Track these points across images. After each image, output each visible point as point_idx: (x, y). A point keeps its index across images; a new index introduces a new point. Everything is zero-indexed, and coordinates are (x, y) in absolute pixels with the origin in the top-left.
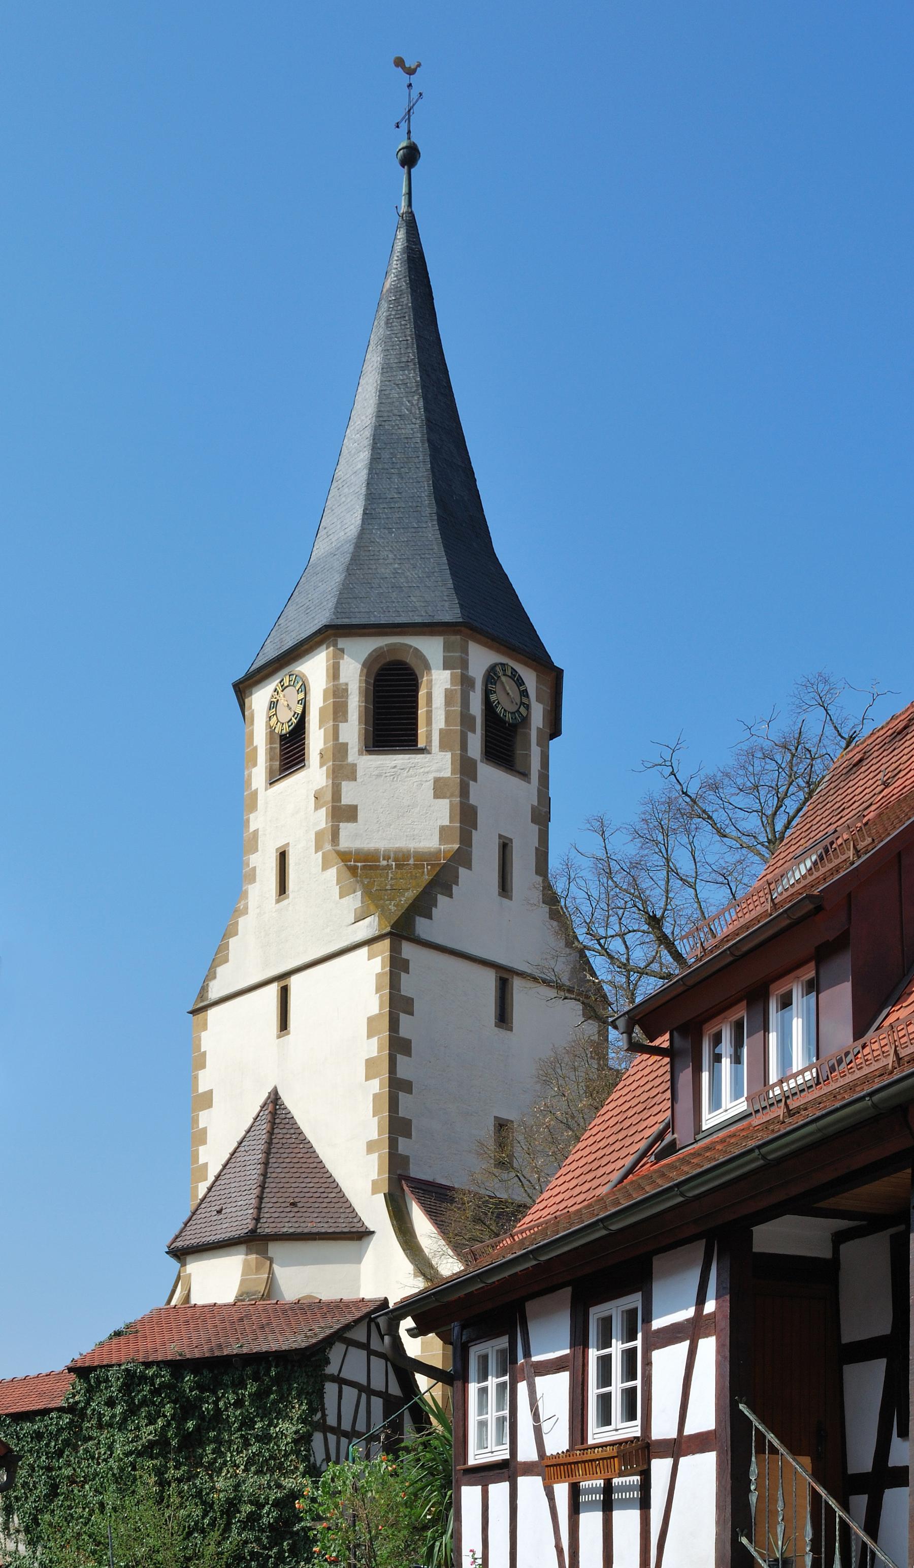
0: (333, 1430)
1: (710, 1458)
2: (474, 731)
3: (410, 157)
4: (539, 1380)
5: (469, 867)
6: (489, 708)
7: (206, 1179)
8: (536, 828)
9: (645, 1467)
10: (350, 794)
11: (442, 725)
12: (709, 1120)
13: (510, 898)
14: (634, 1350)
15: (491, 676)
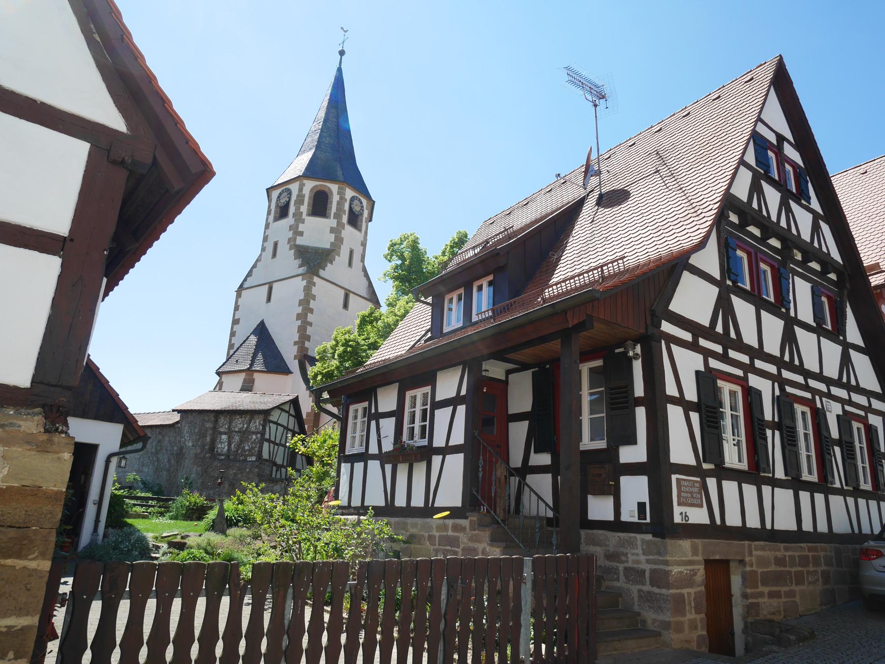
0: (273, 442)
1: (461, 456)
3: (342, 53)
6: (351, 209)
7: (233, 349)
8: (362, 248)
10: (301, 228)
15: (353, 199)
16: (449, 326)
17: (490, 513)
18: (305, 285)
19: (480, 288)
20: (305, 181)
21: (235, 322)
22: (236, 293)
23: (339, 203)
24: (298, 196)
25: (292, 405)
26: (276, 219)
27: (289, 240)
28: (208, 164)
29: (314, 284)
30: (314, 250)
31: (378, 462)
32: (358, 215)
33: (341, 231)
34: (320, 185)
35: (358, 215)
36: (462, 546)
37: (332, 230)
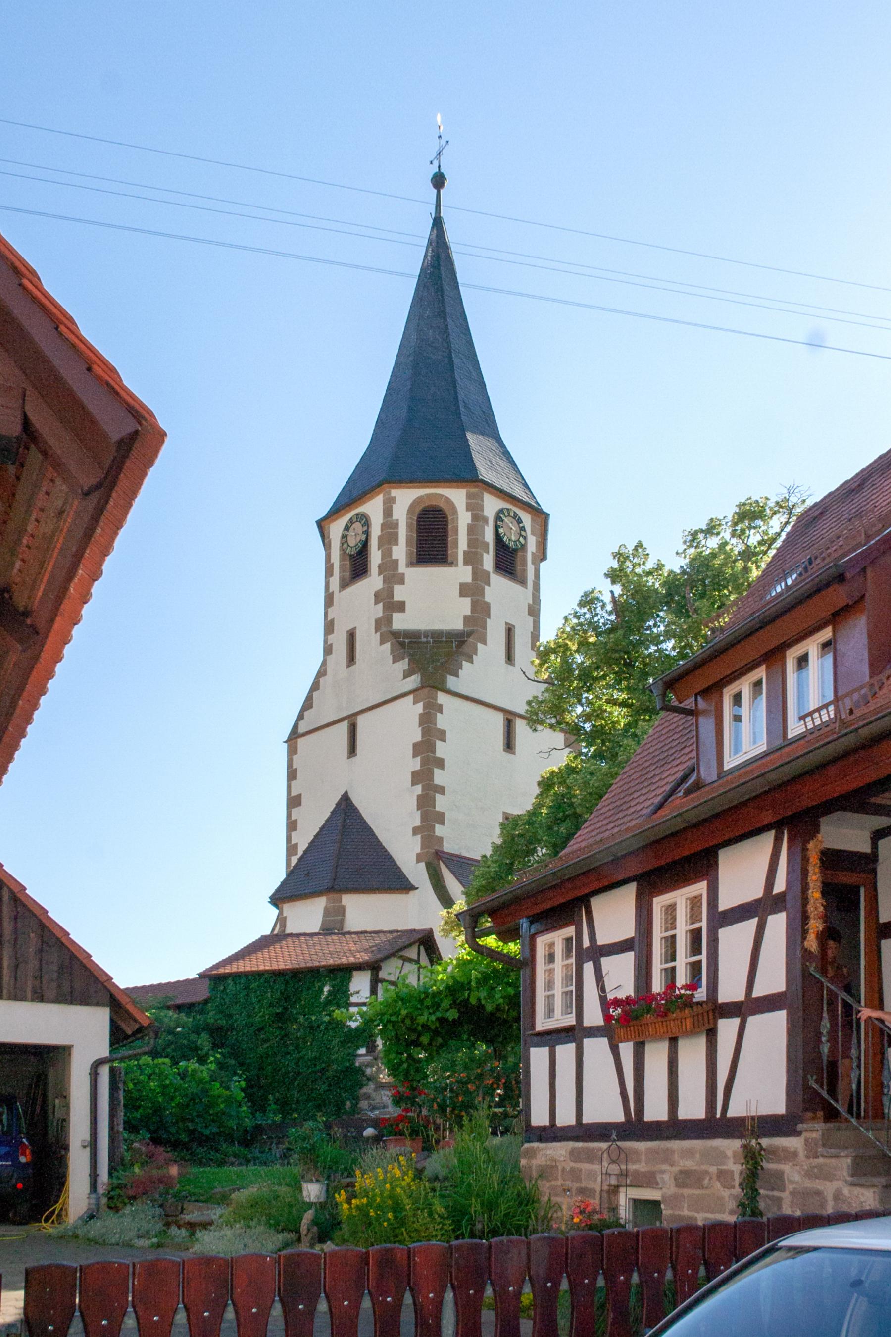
1: (780, 1017)
2: (488, 552)
3: (439, 181)
4: (604, 960)
5: (485, 643)
6: (498, 539)
8: (531, 619)
9: (712, 1026)
10: (399, 593)
11: (466, 548)
12: (730, 762)
13: (513, 665)
14: (699, 930)
15: (498, 518)
16: (736, 752)
17: (850, 1121)
18: (421, 711)
19: (803, 661)
20: (394, 492)
21: (294, 802)
22: (286, 745)
23: (471, 529)
24: (384, 527)
25: (422, 948)
26: (344, 585)
27: (378, 624)
28: (147, 416)
29: (440, 709)
30: (432, 637)
31: (605, 1040)
32: (515, 551)
33: (483, 589)
34: (427, 495)
35: (515, 551)
36: (790, 1188)
37: (464, 590)
